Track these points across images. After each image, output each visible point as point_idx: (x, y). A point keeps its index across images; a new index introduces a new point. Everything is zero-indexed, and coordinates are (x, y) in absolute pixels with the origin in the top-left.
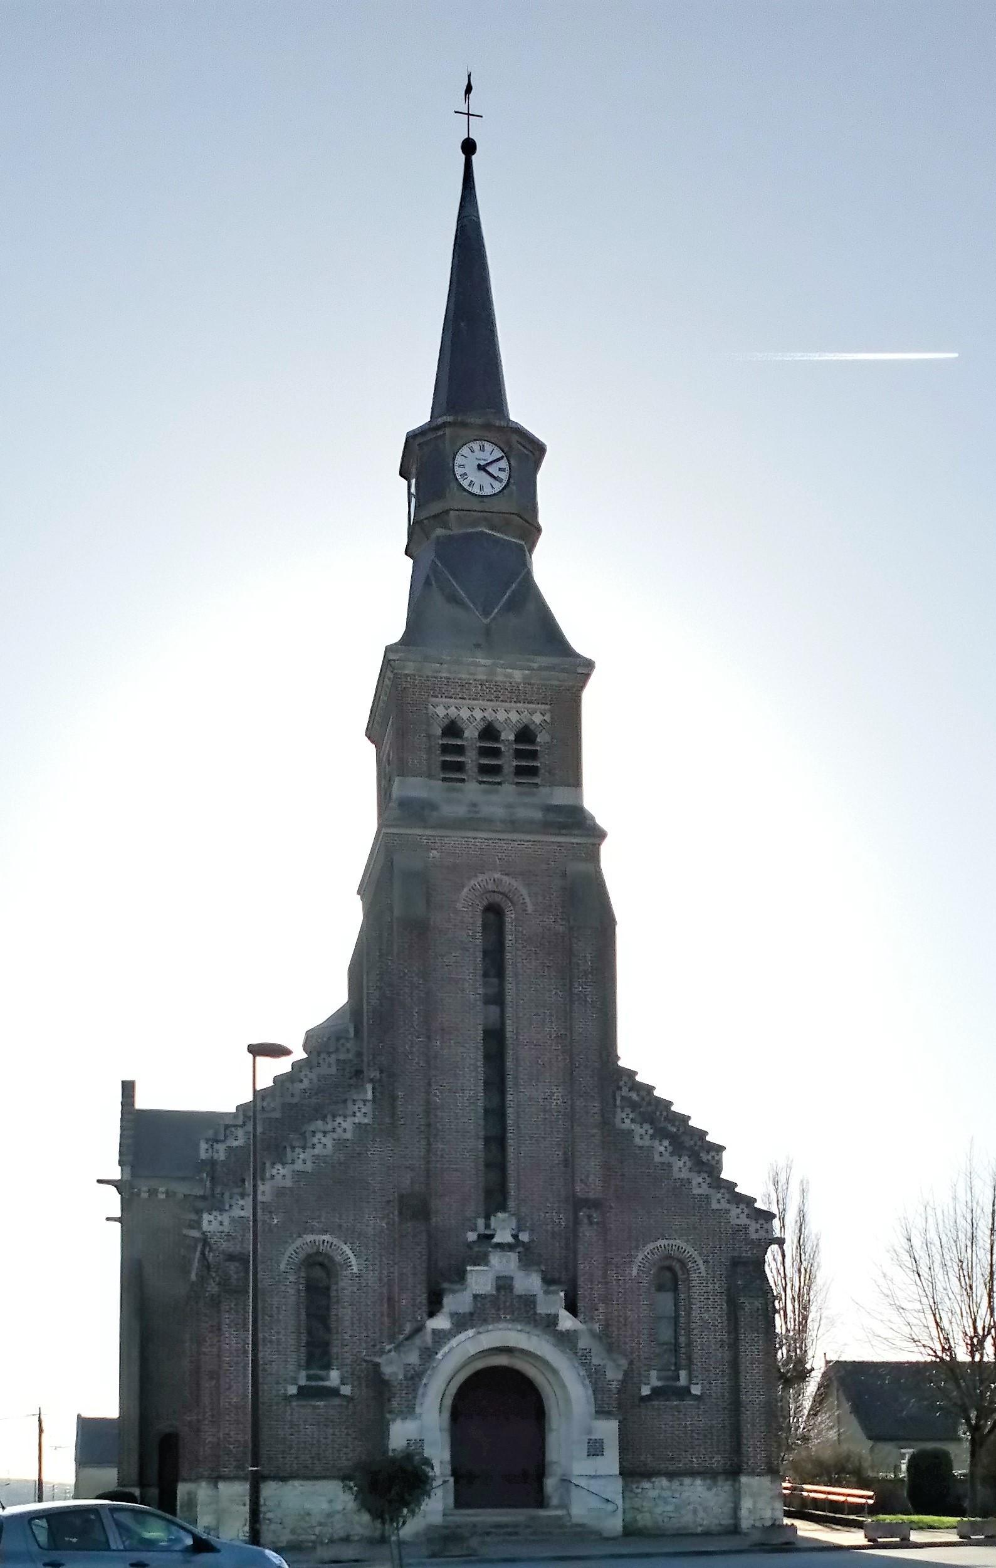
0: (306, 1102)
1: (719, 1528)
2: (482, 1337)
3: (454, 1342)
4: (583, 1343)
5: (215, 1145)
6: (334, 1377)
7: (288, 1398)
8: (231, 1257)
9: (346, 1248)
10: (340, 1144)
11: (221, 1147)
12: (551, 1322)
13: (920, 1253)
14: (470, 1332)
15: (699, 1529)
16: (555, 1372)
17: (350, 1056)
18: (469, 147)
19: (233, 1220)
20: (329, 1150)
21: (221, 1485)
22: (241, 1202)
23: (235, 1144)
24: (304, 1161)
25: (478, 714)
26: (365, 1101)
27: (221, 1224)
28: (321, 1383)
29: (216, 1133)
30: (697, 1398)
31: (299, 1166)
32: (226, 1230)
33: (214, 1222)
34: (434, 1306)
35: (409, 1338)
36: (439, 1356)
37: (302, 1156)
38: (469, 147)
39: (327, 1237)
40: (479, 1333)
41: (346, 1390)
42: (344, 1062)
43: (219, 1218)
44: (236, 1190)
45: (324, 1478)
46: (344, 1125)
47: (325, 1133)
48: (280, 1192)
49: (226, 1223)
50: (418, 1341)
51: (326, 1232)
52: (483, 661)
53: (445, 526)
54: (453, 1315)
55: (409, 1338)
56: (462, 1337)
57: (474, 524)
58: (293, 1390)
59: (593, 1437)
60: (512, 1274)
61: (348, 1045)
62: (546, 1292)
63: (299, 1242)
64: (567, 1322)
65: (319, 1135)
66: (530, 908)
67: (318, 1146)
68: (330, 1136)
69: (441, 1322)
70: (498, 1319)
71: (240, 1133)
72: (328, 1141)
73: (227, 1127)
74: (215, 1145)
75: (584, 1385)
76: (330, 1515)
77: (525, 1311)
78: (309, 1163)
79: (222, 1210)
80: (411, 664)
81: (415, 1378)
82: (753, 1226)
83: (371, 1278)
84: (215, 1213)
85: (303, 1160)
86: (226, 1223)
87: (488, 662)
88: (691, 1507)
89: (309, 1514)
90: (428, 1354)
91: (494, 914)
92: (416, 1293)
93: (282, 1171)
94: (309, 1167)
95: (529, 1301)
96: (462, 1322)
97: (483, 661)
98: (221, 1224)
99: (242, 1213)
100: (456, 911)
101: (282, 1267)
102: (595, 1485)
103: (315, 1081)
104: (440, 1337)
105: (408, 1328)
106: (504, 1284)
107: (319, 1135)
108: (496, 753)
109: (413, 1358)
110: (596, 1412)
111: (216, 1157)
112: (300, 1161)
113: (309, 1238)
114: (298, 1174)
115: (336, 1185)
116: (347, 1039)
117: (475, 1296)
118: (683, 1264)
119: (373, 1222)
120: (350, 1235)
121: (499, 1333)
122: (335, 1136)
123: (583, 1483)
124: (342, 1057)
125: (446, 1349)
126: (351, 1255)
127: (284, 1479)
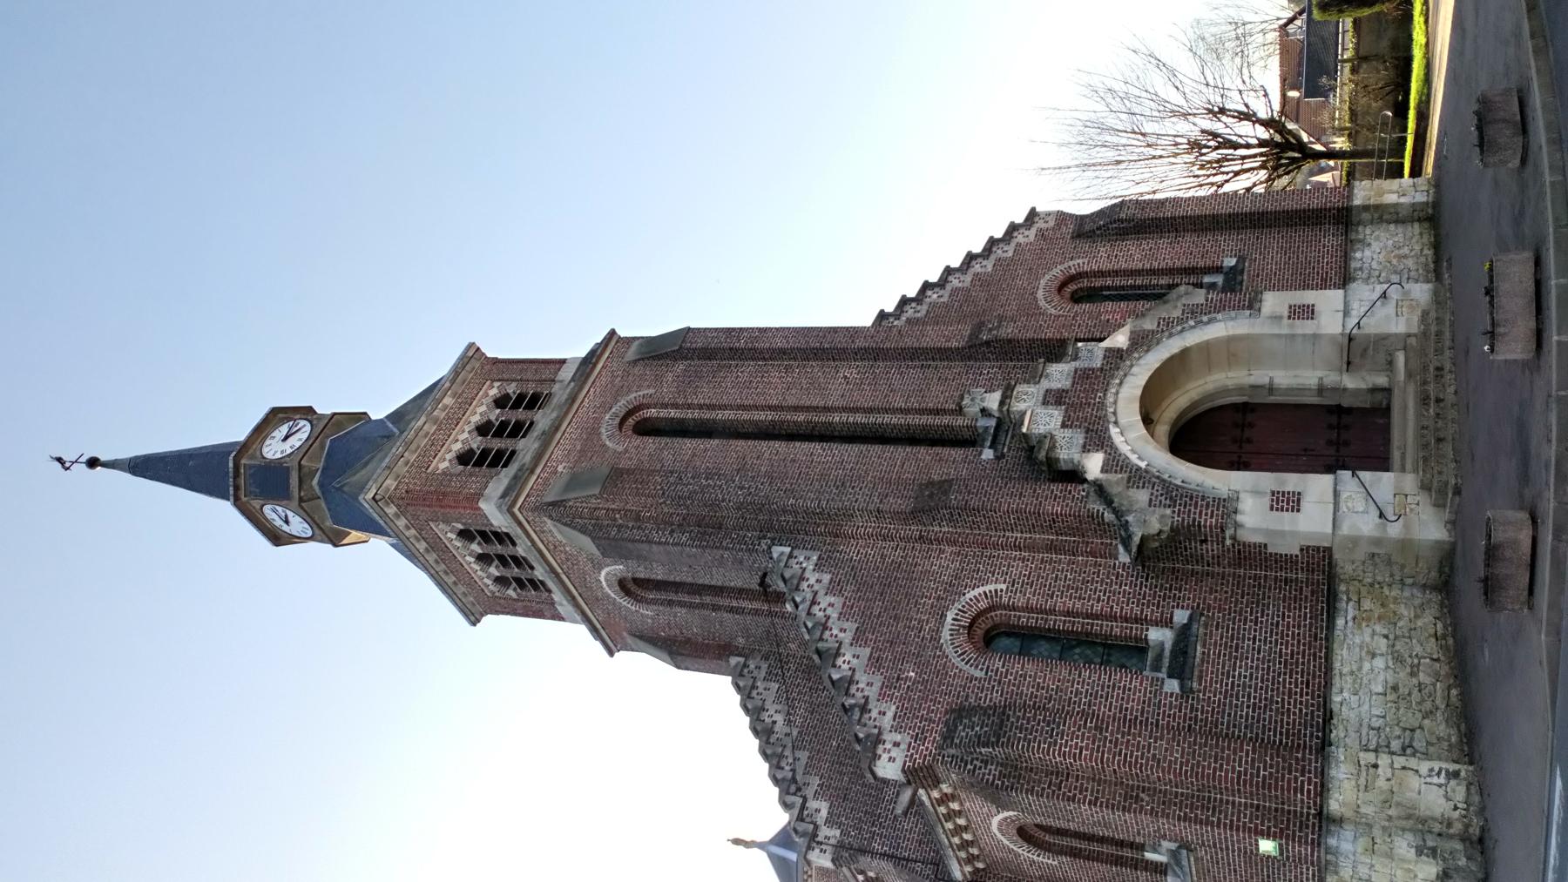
0: (799, 721)
1: (1426, 237)
2: (1122, 421)
3: (1124, 449)
4: (1149, 324)
5: (819, 839)
6: (1156, 635)
7: (1186, 691)
8: (948, 737)
9: (972, 594)
10: (834, 588)
11: (825, 832)
12: (1116, 356)
13: (1111, 155)
14: (1114, 431)
15: (1429, 252)
16: (1185, 353)
17: (765, 666)
18: (93, 463)
19: (896, 729)
20: (838, 601)
21: (1334, 806)
22: (874, 714)
23: (824, 813)
24: (843, 630)
25: (466, 435)
26: (790, 556)
27: (896, 744)
28: (1167, 653)
29: (803, 835)
30: (1241, 259)
31: (847, 637)
32: (908, 739)
33: (893, 754)
34: (1074, 476)
35: (1108, 502)
36: (1143, 465)
37: (835, 632)
38: (93, 463)
39: (950, 616)
40: (1116, 423)
41: (1181, 616)
42: (769, 673)
43: (888, 746)
44: (856, 716)
45: (1328, 658)
46: (812, 581)
47: (814, 602)
48: (875, 663)
49: (898, 738)
50: (1114, 490)
51: (943, 616)
52: (420, 423)
53: (312, 474)
54: (1085, 449)
55: (1108, 502)
56: (1118, 439)
57: (322, 447)
58: (1173, 686)
59: (1286, 314)
60: (1042, 392)
61: (752, 666)
62: (1076, 358)
63: (949, 650)
64: (1120, 339)
65: (815, 609)
66: (651, 391)
67: (829, 611)
68: (819, 598)
69: (1093, 465)
70: (1102, 405)
71: (813, 804)
72: (824, 601)
73: (800, 818)
74: (819, 839)
75: (1210, 321)
76: (1399, 659)
77: (1095, 382)
78: (846, 625)
79: (878, 740)
80: (388, 482)
81: (1171, 493)
82: (1040, 224)
83: (1018, 569)
84: (879, 752)
85: (841, 632)
86: (898, 738)
87: (423, 419)
88: (1395, 262)
89: (1395, 688)
90: (1138, 477)
91: (646, 429)
92: (1054, 500)
93: (847, 657)
94: (851, 626)
95: (1084, 377)
96: (1097, 438)
97: (420, 423)
98: (896, 744)
99: (890, 714)
100: (626, 451)
101: (978, 674)
102: (1357, 309)
103: (779, 707)
104: (1114, 462)
105: (1096, 506)
106: (1054, 398)
107: (815, 609)
108: (504, 425)
109: (1141, 496)
110: (1250, 307)
111: (833, 841)
112: (842, 635)
113: (946, 635)
114: (858, 639)
115: (885, 606)
116: (745, 665)
117: (1064, 426)
118: (1071, 279)
119: (944, 562)
120: (953, 589)
121: (1120, 404)
122: (821, 593)
123: (1352, 322)
124: (763, 674)
125: (1134, 458)
126: (981, 590)
127: (1328, 717)
